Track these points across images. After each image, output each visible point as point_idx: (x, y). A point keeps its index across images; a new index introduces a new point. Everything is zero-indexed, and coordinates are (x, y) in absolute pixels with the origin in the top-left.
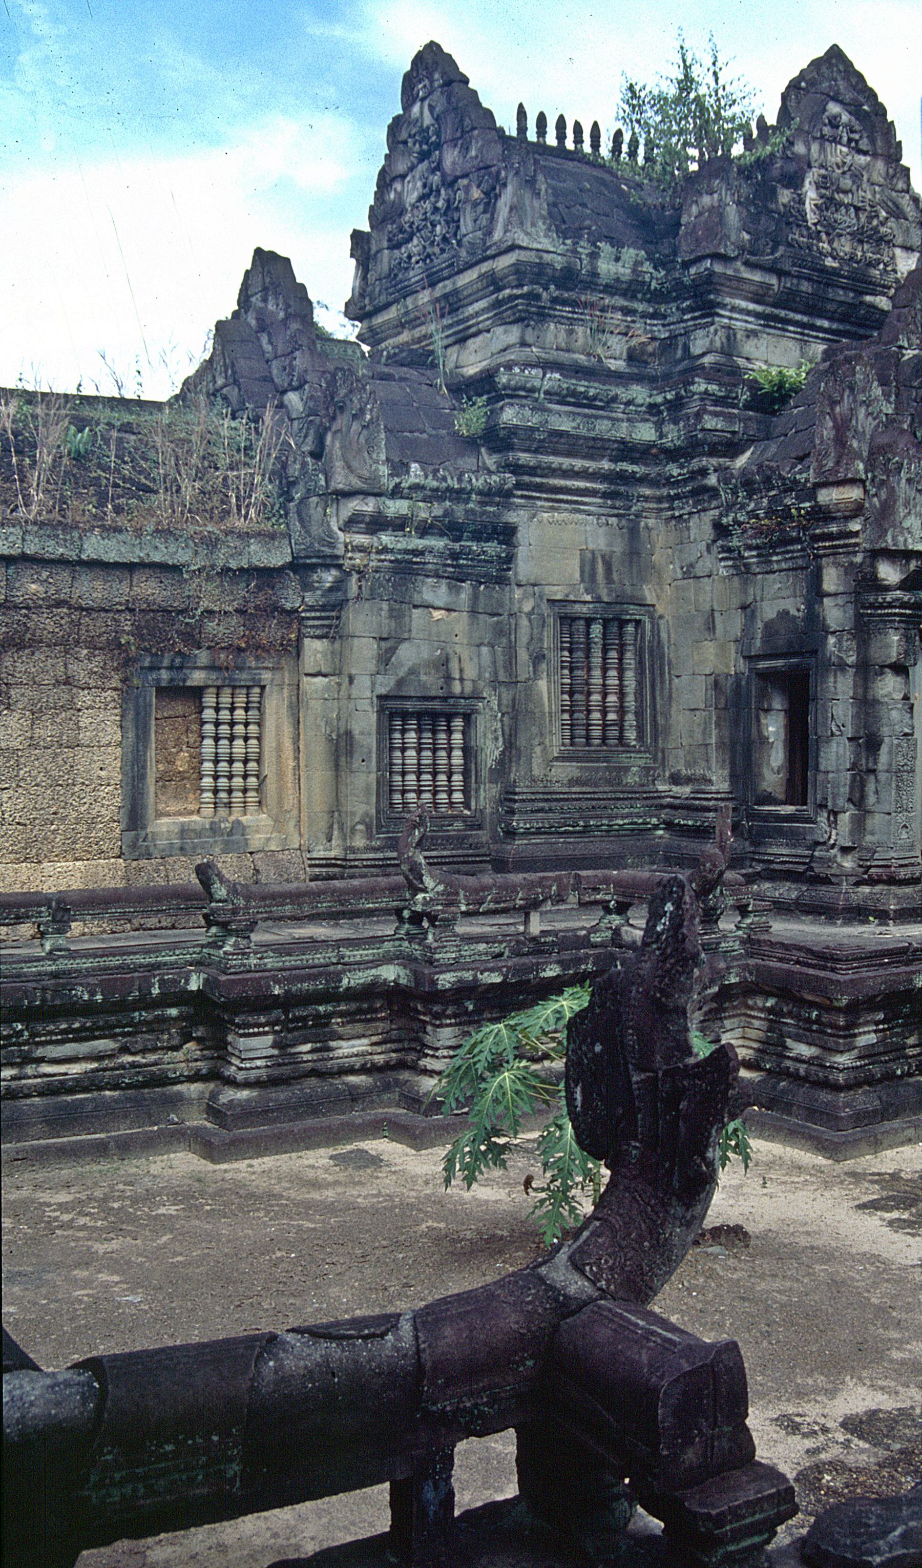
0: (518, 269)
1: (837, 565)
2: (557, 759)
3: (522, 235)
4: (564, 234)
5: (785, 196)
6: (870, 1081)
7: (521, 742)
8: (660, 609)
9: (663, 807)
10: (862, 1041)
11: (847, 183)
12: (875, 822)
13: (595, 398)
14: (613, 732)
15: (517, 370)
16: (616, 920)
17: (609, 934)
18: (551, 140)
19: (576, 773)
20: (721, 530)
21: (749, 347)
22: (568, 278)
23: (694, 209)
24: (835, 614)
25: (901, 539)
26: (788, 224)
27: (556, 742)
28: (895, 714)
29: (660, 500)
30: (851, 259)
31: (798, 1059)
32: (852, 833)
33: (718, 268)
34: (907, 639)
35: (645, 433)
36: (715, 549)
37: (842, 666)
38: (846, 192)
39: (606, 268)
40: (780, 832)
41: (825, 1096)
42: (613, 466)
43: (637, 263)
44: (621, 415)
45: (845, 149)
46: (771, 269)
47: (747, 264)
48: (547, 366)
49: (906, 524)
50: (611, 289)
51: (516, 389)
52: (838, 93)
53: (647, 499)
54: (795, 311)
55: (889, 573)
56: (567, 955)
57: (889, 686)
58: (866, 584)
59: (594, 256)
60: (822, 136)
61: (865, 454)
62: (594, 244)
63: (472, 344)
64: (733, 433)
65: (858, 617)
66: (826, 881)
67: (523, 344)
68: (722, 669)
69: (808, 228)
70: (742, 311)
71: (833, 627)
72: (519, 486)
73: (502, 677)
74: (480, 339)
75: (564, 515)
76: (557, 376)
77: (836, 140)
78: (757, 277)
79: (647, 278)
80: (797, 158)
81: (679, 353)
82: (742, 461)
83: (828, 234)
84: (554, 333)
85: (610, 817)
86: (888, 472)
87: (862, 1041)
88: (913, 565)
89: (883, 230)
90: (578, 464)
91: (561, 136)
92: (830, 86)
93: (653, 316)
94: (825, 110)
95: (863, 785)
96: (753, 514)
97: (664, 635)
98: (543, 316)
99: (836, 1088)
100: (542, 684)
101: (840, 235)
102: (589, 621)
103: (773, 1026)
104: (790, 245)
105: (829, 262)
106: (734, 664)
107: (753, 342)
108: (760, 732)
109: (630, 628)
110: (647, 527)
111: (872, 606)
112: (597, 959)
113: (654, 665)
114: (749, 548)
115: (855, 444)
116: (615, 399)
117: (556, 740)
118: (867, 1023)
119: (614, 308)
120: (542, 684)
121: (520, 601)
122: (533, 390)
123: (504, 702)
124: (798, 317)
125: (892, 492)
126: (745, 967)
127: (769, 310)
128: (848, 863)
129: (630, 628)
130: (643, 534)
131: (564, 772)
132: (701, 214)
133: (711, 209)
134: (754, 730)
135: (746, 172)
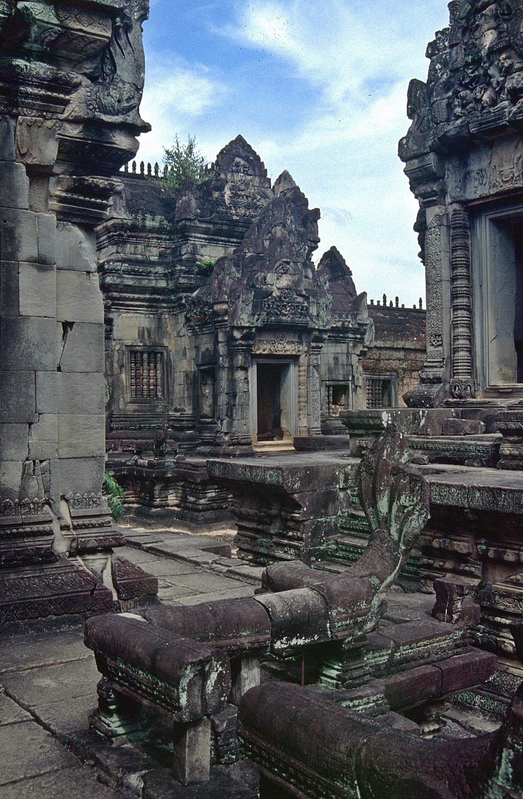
0: (114, 225)
1: (222, 332)
2: (129, 403)
3: (115, 214)
4: (131, 213)
5: (216, 194)
6: (213, 509)
7: (115, 396)
8: (170, 348)
9: (171, 420)
10: (209, 495)
11: (243, 187)
12: (235, 423)
13: (142, 272)
14: (152, 393)
15: (111, 263)
16: (136, 457)
17: (134, 462)
18: (138, 171)
19: (137, 408)
20: (188, 320)
21: (202, 251)
22: (134, 228)
23: (180, 202)
24: (222, 349)
25: (239, 322)
26: (217, 205)
27: (128, 397)
28: (241, 384)
29: (169, 308)
30: (244, 216)
31: (190, 503)
32: (227, 427)
33: (188, 223)
34: (245, 357)
35: (162, 284)
36: (186, 326)
37: (224, 368)
38: (242, 191)
39: (149, 223)
40: (207, 428)
41: (196, 514)
42: (150, 296)
43: (161, 221)
44: (152, 278)
45: (242, 175)
46: (209, 222)
47: (199, 221)
48: (123, 261)
49: (241, 317)
50: (153, 230)
51: (112, 270)
52: (239, 154)
53: (165, 308)
54: (221, 236)
55: (237, 334)
56: (116, 468)
57: (240, 375)
58: (230, 339)
59: (144, 219)
60: (232, 171)
61: (228, 292)
62: (143, 215)
63: (103, 251)
64: (191, 284)
65: (229, 349)
66: (219, 445)
67: (117, 252)
68: (189, 369)
69: (226, 205)
70: (199, 238)
71: (221, 354)
72: (113, 304)
73: (109, 373)
74: (105, 249)
75: (132, 315)
76: (127, 265)
77: (238, 172)
78: (204, 225)
79: (165, 226)
80: (221, 180)
81: (178, 254)
82: (195, 294)
83: (234, 207)
84: (129, 248)
85: (150, 424)
86: (235, 299)
87: (209, 495)
88: (245, 331)
89: (258, 203)
90: (136, 296)
91: (142, 169)
92: (236, 152)
93: (169, 240)
94: (234, 160)
95: (232, 411)
96: (195, 314)
97: (171, 357)
98: (125, 242)
99: (199, 511)
100: (123, 376)
101: (239, 207)
102: (142, 353)
103: (184, 491)
104: (218, 213)
105: (235, 218)
106: (193, 368)
107: (204, 249)
108: (202, 393)
109: (159, 355)
110: (165, 318)
111: (233, 346)
112: (128, 470)
113: (169, 368)
114: (196, 326)
115: (224, 289)
116: (150, 272)
117: (129, 395)
118: (211, 489)
119: (153, 238)
120: (123, 376)
121: (115, 346)
122: (118, 270)
123: (110, 381)
124: (223, 239)
125: (236, 306)
126: (174, 472)
127: (210, 237)
128: (227, 438)
129: (159, 355)
130: (164, 321)
131: (131, 407)
132: (182, 203)
133: (186, 202)
134: (200, 391)
135: (200, 188)
